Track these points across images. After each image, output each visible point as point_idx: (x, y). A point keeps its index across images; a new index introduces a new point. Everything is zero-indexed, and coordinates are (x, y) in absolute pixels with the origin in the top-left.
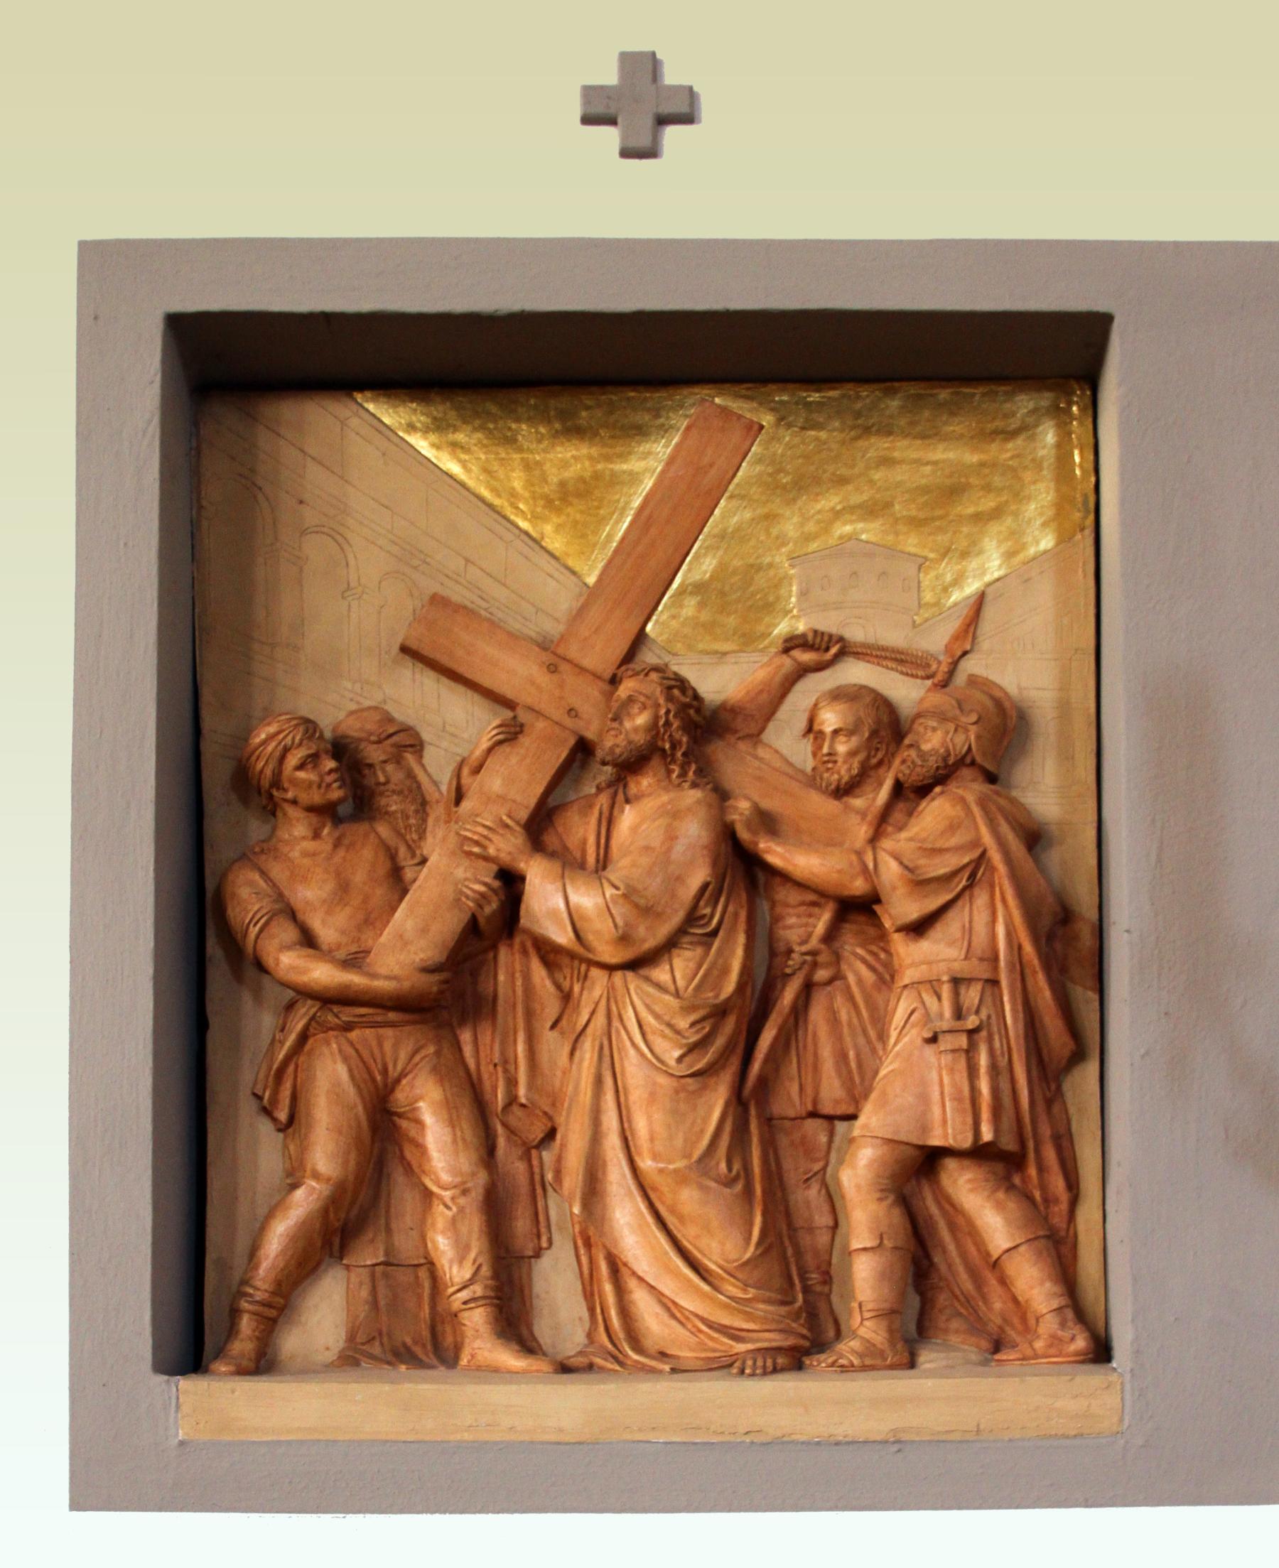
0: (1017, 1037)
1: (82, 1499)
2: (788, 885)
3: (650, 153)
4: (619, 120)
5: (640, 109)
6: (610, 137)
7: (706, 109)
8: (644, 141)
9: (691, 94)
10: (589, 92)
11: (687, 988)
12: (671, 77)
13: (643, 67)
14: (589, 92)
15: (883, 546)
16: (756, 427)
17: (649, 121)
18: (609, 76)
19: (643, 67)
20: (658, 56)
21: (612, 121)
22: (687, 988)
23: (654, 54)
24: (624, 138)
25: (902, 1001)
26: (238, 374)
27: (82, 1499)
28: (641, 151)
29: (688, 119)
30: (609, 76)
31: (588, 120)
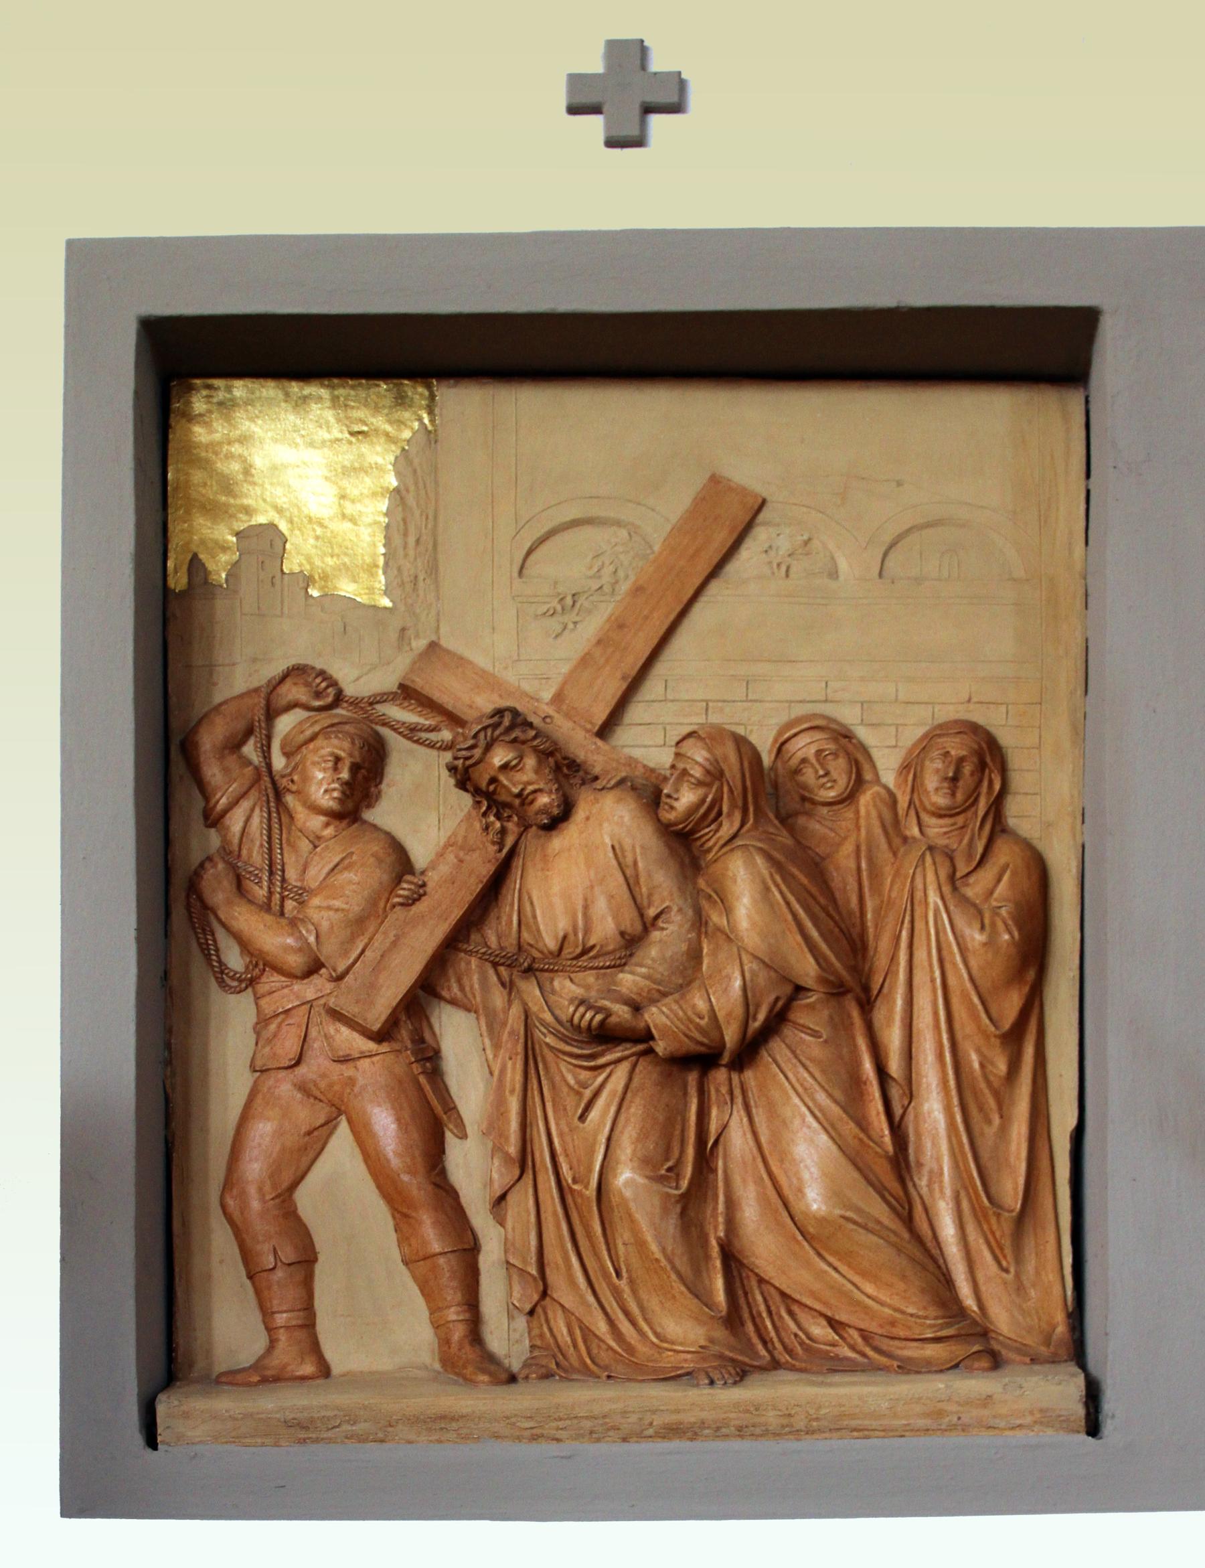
0: (420, 714)
1: (69, 1510)
2: (215, 540)
3: (638, 142)
4: (605, 109)
5: (629, 98)
6: (595, 125)
7: (694, 99)
8: (633, 131)
9: (682, 85)
10: (576, 81)
11: (619, 1061)
12: (657, 64)
13: (629, 55)
14: (576, 81)
15: (274, 782)
16: (317, 843)
17: (636, 111)
18: (595, 64)
19: (629, 55)
20: (646, 44)
21: (595, 110)
22: (619, 1061)
23: (642, 41)
24: (608, 126)
25: (841, 1112)
26: (191, 352)
27: (69, 1510)
28: (625, 140)
29: (676, 108)
30: (595, 64)
31: (573, 110)
